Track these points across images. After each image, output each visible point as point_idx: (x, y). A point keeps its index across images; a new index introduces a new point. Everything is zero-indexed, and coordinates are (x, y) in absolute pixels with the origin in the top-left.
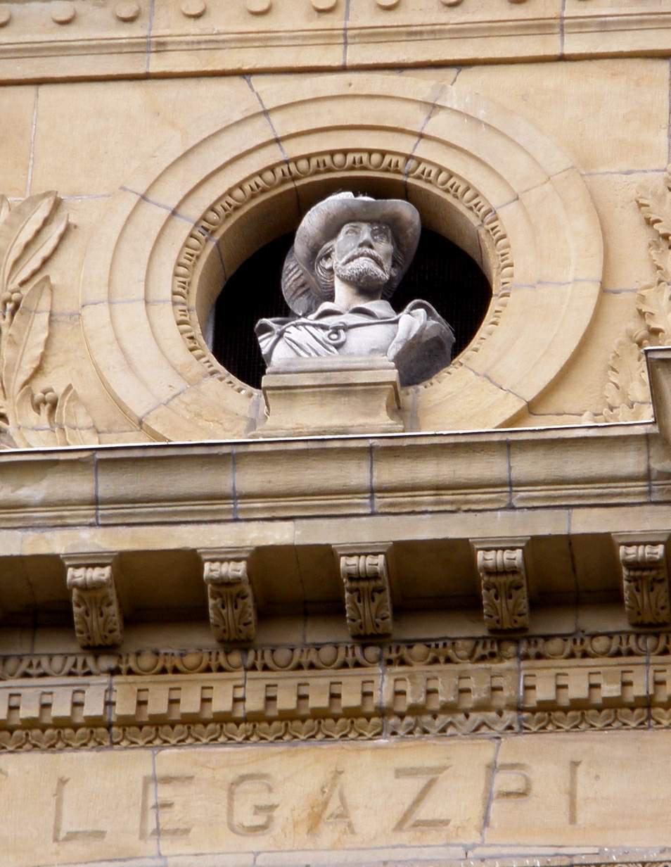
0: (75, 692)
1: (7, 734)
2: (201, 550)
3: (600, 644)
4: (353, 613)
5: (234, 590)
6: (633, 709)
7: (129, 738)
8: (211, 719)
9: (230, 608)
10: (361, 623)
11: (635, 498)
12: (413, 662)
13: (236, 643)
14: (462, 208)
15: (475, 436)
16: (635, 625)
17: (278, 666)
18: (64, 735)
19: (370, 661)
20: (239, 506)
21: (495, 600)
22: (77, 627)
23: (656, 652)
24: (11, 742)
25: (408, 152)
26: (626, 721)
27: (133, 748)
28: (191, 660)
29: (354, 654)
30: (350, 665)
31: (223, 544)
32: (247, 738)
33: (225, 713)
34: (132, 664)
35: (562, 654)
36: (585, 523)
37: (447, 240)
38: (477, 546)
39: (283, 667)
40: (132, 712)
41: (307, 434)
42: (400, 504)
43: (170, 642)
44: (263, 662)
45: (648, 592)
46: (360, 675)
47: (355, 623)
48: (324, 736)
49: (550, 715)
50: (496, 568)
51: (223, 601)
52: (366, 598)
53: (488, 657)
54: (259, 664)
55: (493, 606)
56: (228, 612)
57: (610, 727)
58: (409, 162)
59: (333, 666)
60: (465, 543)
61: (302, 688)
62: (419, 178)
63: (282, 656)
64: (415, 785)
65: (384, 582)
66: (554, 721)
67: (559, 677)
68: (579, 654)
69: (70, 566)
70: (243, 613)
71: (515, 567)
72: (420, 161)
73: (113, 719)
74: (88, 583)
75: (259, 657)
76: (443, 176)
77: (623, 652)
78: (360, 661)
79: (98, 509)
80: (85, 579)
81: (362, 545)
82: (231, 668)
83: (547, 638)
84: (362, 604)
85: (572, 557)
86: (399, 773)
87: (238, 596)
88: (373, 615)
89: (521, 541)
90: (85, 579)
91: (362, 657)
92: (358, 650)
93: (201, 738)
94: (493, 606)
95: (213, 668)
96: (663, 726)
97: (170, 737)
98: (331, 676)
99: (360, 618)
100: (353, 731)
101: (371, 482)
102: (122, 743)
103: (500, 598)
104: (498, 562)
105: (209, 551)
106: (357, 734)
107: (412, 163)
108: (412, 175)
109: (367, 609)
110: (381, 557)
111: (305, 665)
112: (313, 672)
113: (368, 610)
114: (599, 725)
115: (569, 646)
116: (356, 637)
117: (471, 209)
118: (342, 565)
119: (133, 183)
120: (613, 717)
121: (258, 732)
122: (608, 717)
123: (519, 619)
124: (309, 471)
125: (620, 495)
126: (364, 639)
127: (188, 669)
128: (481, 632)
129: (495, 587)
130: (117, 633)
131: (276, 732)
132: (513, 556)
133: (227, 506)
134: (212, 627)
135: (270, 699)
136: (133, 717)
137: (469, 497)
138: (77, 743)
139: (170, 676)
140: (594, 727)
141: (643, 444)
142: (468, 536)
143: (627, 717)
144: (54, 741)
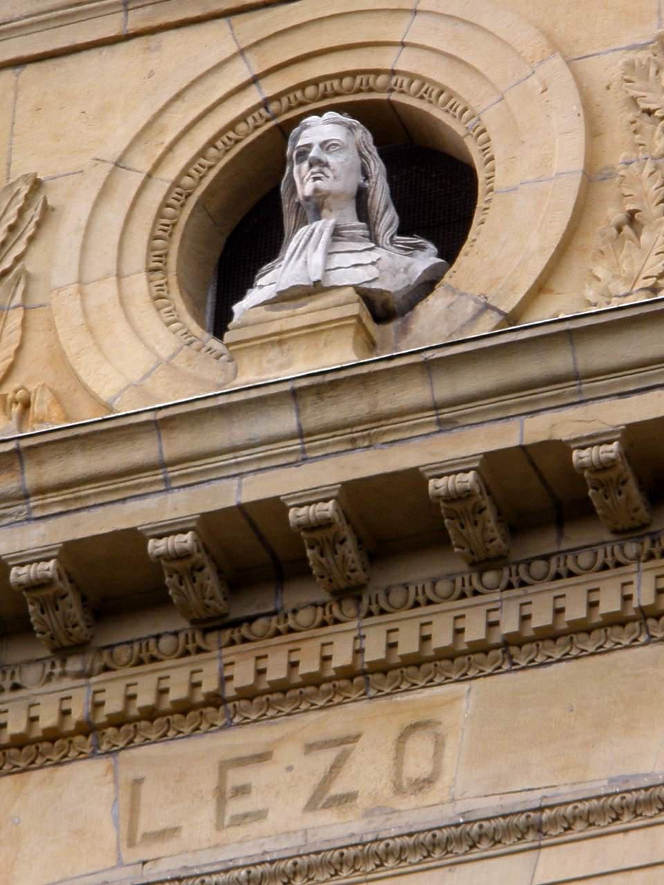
0: (258, 658)
2: (6, 557)
3: (585, 559)
4: (39, 626)
5: (329, 533)
9: (50, 611)
11: (201, 477)
12: (118, 667)
13: (349, 593)
15: (183, 406)
16: (615, 532)
18: (10, 755)
19: (488, 586)
20: (171, 474)
21: (461, 530)
22: (599, 512)
23: (176, 655)
26: (415, 681)
27: (516, 670)
28: (443, 587)
30: (146, 661)
31: (164, 514)
33: (118, 714)
34: (291, 622)
35: (545, 578)
36: (255, 489)
37: (280, 244)
38: (428, 474)
39: (542, 579)
40: (482, 636)
42: (508, 407)
43: (420, 572)
44: (195, 645)
45: (191, 583)
47: (45, 636)
48: (376, 691)
50: (168, 552)
51: (606, 491)
52: (49, 607)
53: (193, 653)
54: (609, 559)
55: (43, 622)
56: (187, 588)
59: (594, 569)
60: (133, 532)
61: (525, 607)
63: (397, 598)
64: (327, 758)
65: (200, 557)
66: (241, 713)
67: (524, 607)
68: (564, 574)
69: (576, 448)
70: (484, 529)
71: (187, 551)
75: (328, 613)
77: (610, 565)
78: (338, 617)
79: (581, 384)
80: (29, 576)
81: (184, 519)
82: (391, 610)
83: (251, 620)
84: (46, 615)
86: (310, 748)
87: (193, 569)
88: (62, 624)
90: (29, 576)
91: (576, 567)
93: (216, 723)
94: (43, 622)
95: (515, 584)
98: (587, 582)
99: (49, 630)
100: (438, 675)
101: (433, 397)
102: (70, 755)
103: (46, 611)
104: (450, 488)
105: (293, 495)
106: (309, 705)
109: (53, 618)
110: (331, 503)
111: (564, 574)
113: (54, 620)
114: (153, 737)
115: (274, 623)
116: (55, 651)
118: (12, 578)
119: (127, 122)
121: (407, 678)
123: (353, 575)
125: (396, 430)
129: (177, 572)
130: (499, 541)
132: (465, 480)
134: (601, 518)
135: (359, 652)
136: (251, 686)
137: (78, 494)
141: (290, 400)
142: (278, 494)
144: (131, 736)
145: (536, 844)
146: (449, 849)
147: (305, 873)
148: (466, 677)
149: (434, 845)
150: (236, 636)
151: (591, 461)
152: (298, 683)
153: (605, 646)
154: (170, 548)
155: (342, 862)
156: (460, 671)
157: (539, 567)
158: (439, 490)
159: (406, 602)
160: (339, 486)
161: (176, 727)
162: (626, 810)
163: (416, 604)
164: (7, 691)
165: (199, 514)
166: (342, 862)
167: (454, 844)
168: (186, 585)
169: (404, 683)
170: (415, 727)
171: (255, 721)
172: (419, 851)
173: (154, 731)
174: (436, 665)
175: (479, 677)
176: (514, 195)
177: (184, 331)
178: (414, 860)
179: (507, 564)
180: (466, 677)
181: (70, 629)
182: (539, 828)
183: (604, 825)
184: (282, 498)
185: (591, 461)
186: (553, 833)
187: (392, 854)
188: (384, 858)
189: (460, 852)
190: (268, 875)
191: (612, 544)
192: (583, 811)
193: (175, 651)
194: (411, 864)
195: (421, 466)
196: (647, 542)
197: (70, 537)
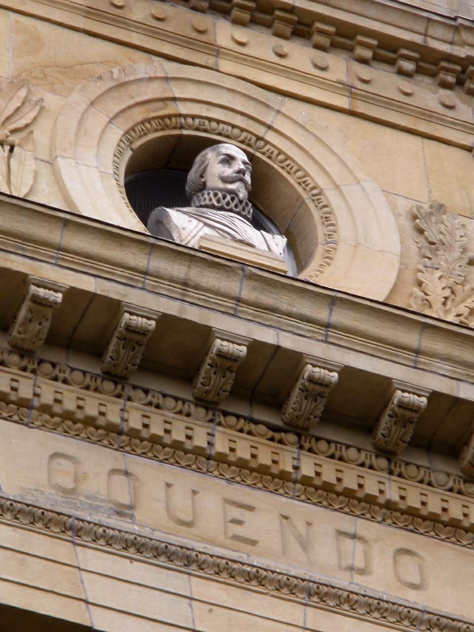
1: (4, 404)
2: (124, 303)
6: (445, 526)
7: (457, 537)
8: (169, 444)
10: (117, 364)
13: (207, 404)
14: (291, 180)
16: (196, 398)
17: (227, 425)
24: (250, 479)
25: (261, 135)
29: (371, 459)
32: (384, 520)
35: (265, 436)
36: (288, 342)
41: (227, 269)
46: (98, 399)
49: (391, 513)
57: (55, 431)
58: (258, 142)
62: (263, 153)
72: (267, 143)
73: (126, 430)
74: (325, 380)
76: (281, 157)
79: (327, 331)
82: (348, 461)
84: (215, 376)
85: (83, 316)
88: (220, 387)
89: (156, 315)
92: (373, 458)
96: (301, 499)
97: (420, 528)
105: (402, 382)
107: (262, 143)
108: (259, 150)
112: (157, 410)
117: (300, 184)
120: (452, 534)
121: (457, 535)
122: (449, 533)
124: (270, 303)
126: (108, 375)
127: (351, 461)
128: (98, 372)
131: (99, 436)
133: (63, 255)
138: (315, 499)
139: (425, 486)
140: (332, 506)
143: (354, 506)
144: (191, 463)
145: (70, 539)
146: (49, 525)
147: (14, 513)
148: (406, 528)
149: (8, 509)
150: (246, 428)
151: (228, 351)
152: (423, 515)
153: (125, 448)
154: (139, 325)
155: (42, 518)
156: (9, 412)
157: (323, 445)
158: (131, 321)
159: (174, 408)
160: (431, 391)
161: (373, 514)
162: (226, 571)
163: (421, 482)
164: (60, 381)
165: (432, 390)
166: (42, 518)
167: (389, 613)
168: (217, 377)
169: (347, 507)
170: (127, 473)
171: (227, 479)
172: (29, 518)
173: (316, 497)
174: (305, 489)
175: (273, 493)
176: (144, 88)
177: (117, 165)
178: (331, 604)
179: (213, 409)
180: (406, 528)
181: (312, 417)
182: (322, 597)
183: (178, 564)
184: (214, 329)
185: (228, 351)
186: (85, 538)
187: (43, 520)
188: (37, 519)
189: (269, 588)
190: (390, 610)
191: (92, 375)
192: (412, 615)
193: (174, 408)
194: (206, 573)
195: (394, 379)
196: (120, 387)
197: (74, 285)
